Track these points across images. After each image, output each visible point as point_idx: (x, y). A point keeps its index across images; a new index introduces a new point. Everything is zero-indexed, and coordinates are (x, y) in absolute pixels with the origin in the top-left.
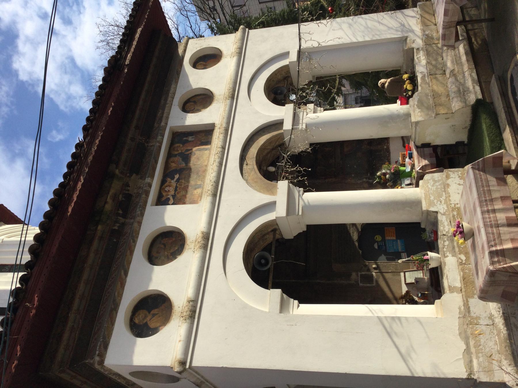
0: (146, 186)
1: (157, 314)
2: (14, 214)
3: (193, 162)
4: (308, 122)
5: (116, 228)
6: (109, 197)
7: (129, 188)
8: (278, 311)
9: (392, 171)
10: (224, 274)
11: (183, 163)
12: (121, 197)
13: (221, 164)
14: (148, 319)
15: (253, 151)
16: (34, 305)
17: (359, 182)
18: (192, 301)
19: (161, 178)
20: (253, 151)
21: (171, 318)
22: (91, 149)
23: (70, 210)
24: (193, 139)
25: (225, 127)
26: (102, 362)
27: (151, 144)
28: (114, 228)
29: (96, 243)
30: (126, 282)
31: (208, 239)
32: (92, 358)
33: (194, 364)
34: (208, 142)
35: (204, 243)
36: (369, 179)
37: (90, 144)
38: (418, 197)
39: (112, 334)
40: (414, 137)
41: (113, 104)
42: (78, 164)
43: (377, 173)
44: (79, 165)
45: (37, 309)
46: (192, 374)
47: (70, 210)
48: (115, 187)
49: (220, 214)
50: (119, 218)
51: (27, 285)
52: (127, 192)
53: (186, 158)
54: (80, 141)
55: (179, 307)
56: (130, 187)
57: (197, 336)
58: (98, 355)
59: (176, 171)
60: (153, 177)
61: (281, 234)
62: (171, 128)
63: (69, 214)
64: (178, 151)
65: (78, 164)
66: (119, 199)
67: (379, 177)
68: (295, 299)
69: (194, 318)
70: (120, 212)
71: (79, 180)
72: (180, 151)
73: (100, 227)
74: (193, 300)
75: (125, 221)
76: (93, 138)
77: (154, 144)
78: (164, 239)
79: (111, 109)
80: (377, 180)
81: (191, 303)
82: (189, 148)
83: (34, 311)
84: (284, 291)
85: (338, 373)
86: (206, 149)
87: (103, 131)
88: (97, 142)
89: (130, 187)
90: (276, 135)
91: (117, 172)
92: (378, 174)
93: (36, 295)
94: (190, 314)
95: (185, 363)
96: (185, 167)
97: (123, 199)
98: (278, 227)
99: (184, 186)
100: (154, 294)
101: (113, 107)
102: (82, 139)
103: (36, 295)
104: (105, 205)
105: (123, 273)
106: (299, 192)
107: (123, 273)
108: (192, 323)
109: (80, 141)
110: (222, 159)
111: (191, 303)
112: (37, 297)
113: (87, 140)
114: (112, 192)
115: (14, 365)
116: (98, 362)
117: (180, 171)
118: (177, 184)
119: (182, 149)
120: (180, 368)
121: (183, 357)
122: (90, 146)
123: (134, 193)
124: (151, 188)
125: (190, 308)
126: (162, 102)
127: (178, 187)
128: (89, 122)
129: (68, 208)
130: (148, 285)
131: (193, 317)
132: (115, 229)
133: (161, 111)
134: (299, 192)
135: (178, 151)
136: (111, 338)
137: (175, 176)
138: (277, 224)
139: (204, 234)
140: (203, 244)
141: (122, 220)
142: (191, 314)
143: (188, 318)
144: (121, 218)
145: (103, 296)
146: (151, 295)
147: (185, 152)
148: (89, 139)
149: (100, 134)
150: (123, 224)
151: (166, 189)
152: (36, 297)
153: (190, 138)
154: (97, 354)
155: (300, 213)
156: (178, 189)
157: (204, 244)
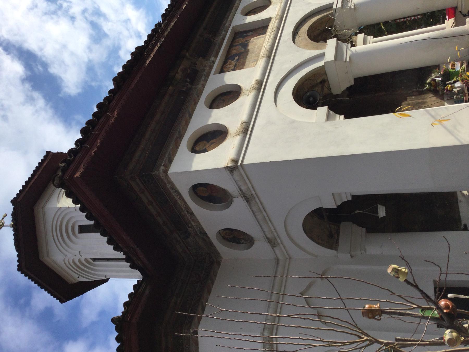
0: (210, 62)
1: (215, 142)
2: (106, 282)
3: (250, 47)
4: (356, 3)
5: (184, 90)
6: (179, 70)
7: (196, 65)
8: (325, 120)
9: (441, 73)
10: (275, 105)
11: (243, 49)
12: (189, 71)
13: (275, 38)
14: (207, 146)
15: (306, 27)
16: (114, 116)
17: (409, 92)
18: (245, 122)
19: (223, 60)
20: (306, 27)
21: (226, 138)
22: (167, 28)
23: (148, 62)
24: (252, 34)
25: (280, 15)
26: (166, 171)
27: (216, 40)
28: (182, 90)
29: (166, 98)
30: (190, 122)
31: (262, 85)
32: (159, 170)
33: (245, 162)
34: (265, 33)
35: (258, 87)
36: (419, 88)
37: (167, 25)
38: (465, 29)
39: (176, 154)
40: (460, 5)
41: (187, 3)
42: (156, 36)
43: (427, 80)
44: (157, 37)
45: (116, 119)
46: (243, 178)
47: (148, 62)
48: (185, 64)
49: (273, 69)
50: (187, 84)
51: (109, 103)
52: (194, 68)
53: (245, 45)
54: (158, 22)
55: (234, 131)
56: (197, 65)
57: (247, 149)
58: (164, 166)
59: (236, 55)
60: (216, 56)
61: (329, 88)
62: (233, 27)
63: (146, 65)
64: (238, 42)
65: (156, 36)
66: (187, 72)
67: (430, 84)
68: (341, 115)
69: (247, 134)
70: (188, 80)
71: (156, 44)
72: (240, 42)
73: (171, 88)
74: (246, 122)
75: (191, 87)
76: (170, 22)
77: (218, 39)
78: (223, 97)
79: (185, 5)
80: (427, 87)
81: (244, 124)
82: (248, 39)
83: (113, 120)
84: (330, 109)
85: (383, 152)
86: (263, 37)
87: (178, 18)
88: (172, 24)
89: (197, 65)
90: (327, 16)
91: (187, 54)
92: (428, 81)
93: (116, 111)
94: (243, 130)
95: (237, 162)
96: (244, 51)
97: (191, 72)
98: (327, 77)
99: (243, 63)
100: (213, 131)
101: (187, 5)
102: (161, 21)
103: (116, 111)
104: (176, 74)
105: (187, 116)
106: (347, 46)
107: (187, 116)
108: (245, 137)
109: (158, 22)
110: (277, 35)
111: (244, 124)
112: (117, 112)
113: (164, 23)
114: (182, 67)
115: (93, 151)
116: (163, 170)
117: (240, 54)
118: (236, 62)
119: (243, 40)
120: (232, 164)
121: (235, 157)
122: (166, 27)
123: (200, 70)
124: (214, 64)
125: (243, 127)
126: (228, 14)
127: (237, 64)
128: (167, 11)
129: (146, 62)
130: (208, 120)
131: (246, 133)
132: (183, 91)
133: (226, 20)
134: (347, 46)
135: (238, 42)
136: (175, 156)
137: (235, 58)
138: (326, 74)
139: (258, 81)
140: (257, 87)
141: (189, 86)
142: (244, 131)
143: (241, 133)
144: (188, 84)
145: (171, 132)
146: (210, 132)
147: (245, 42)
148: (166, 22)
149: (175, 19)
150: (190, 89)
151: (227, 67)
152: (115, 112)
153: (250, 34)
154: (163, 165)
155: (348, 60)
156: (237, 65)
157: (258, 87)
